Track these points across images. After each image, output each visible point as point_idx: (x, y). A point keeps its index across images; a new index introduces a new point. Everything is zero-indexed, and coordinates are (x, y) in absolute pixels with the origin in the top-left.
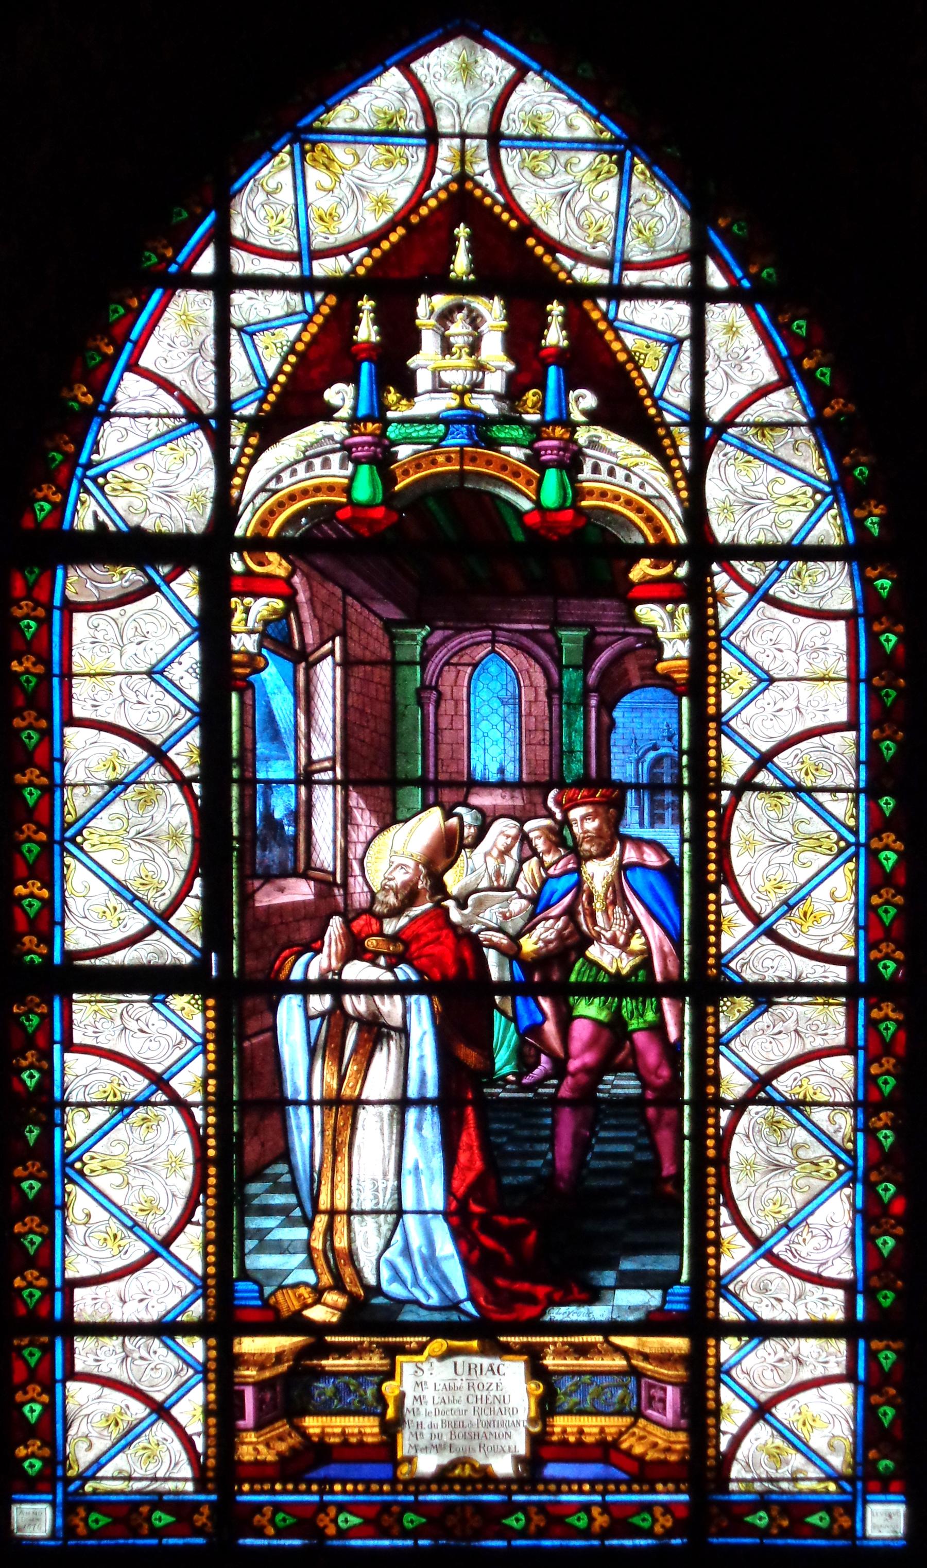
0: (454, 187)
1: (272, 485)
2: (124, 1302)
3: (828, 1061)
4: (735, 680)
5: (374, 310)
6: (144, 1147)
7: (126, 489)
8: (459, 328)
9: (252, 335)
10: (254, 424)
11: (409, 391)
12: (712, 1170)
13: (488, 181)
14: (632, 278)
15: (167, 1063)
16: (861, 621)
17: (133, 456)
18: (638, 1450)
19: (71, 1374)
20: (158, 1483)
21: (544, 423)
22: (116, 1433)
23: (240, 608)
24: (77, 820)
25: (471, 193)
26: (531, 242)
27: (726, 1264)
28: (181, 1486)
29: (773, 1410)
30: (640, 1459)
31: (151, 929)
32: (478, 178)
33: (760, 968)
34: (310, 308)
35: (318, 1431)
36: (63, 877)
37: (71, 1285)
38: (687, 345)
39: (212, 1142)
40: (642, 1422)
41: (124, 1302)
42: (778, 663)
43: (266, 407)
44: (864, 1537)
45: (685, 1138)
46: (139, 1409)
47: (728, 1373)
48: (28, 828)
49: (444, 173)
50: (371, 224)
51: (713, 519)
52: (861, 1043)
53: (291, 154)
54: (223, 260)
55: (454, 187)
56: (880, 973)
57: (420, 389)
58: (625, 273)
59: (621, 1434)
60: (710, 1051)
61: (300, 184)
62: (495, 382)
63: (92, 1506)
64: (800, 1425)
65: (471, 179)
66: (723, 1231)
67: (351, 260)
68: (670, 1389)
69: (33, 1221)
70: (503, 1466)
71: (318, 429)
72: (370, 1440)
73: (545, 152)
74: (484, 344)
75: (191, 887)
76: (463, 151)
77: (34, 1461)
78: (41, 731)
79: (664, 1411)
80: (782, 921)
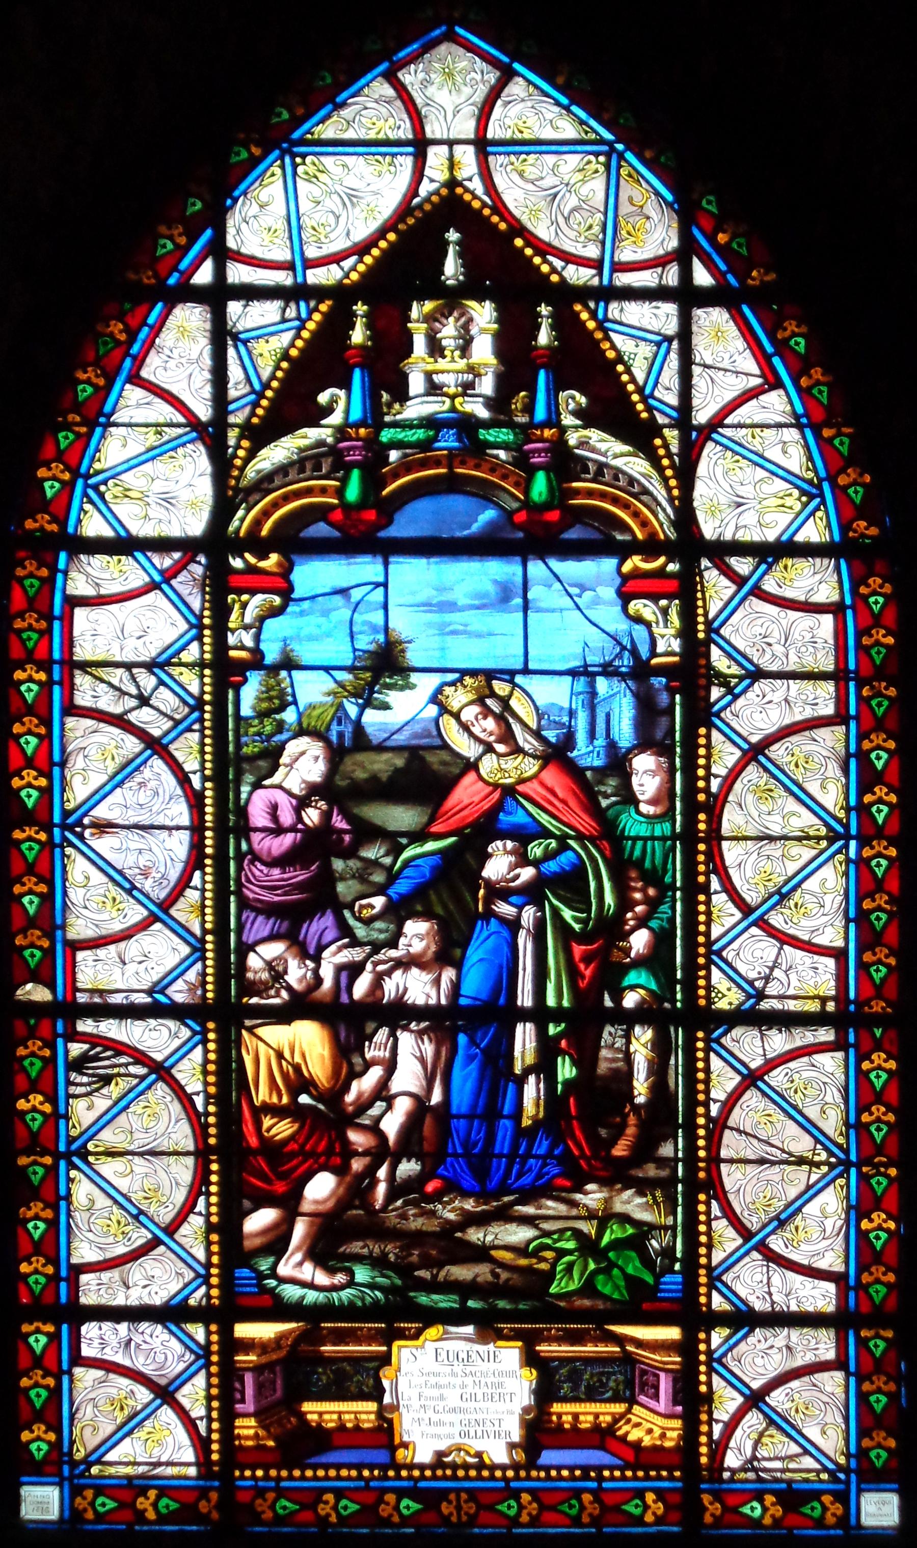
0: (444, 192)
1: (265, 485)
2: (125, 964)
3: (819, 1058)
4: (724, 996)
5: (366, 315)
6: (143, 811)
7: (127, 496)
8: (449, 331)
9: (245, 342)
10: (247, 429)
11: (402, 395)
12: (702, 847)
13: (477, 186)
14: (624, 279)
15: (167, 1052)
16: (849, 613)
17: (132, 465)
18: (633, 1436)
19: (77, 1359)
20: (163, 1468)
21: (532, 425)
22: (120, 1417)
23: (237, 606)
24: (82, 1134)
25: (461, 197)
26: (519, 242)
27: (718, 1256)
28: (184, 1471)
29: (766, 751)
30: (637, 1444)
31: (152, 919)
32: (466, 183)
33: (749, 1282)
34: (304, 315)
35: (315, 1417)
36: (64, 867)
37: (79, 1270)
38: (675, 345)
39: (212, 1131)
40: (636, 1409)
41: (128, 1288)
42: (768, 656)
43: (260, 411)
44: (859, 1526)
45: (677, 982)
46: (144, 1395)
47: (719, 1361)
48: (31, 721)
49: (432, 181)
50: (361, 233)
51: (700, 516)
52: (853, 711)
53: (283, 167)
54: (220, 272)
55: (444, 192)
56: (873, 1463)
57: (412, 393)
58: (615, 275)
59: (616, 1420)
60: (701, 772)
61: (291, 194)
62: (487, 386)
63: (100, 1490)
64: (792, 767)
65: (460, 184)
66: (714, 1224)
67: (342, 269)
68: (662, 1375)
69: (31, 721)
70: (498, 1454)
71: (311, 435)
72: (366, 1425)
73: (532, 156)
74: (475, 346)
75: (195, 1205)
76: (451, 158)
77: (30, 738)
78: (41, 632)
79: (656, 1397)
80: (773, 1237)
